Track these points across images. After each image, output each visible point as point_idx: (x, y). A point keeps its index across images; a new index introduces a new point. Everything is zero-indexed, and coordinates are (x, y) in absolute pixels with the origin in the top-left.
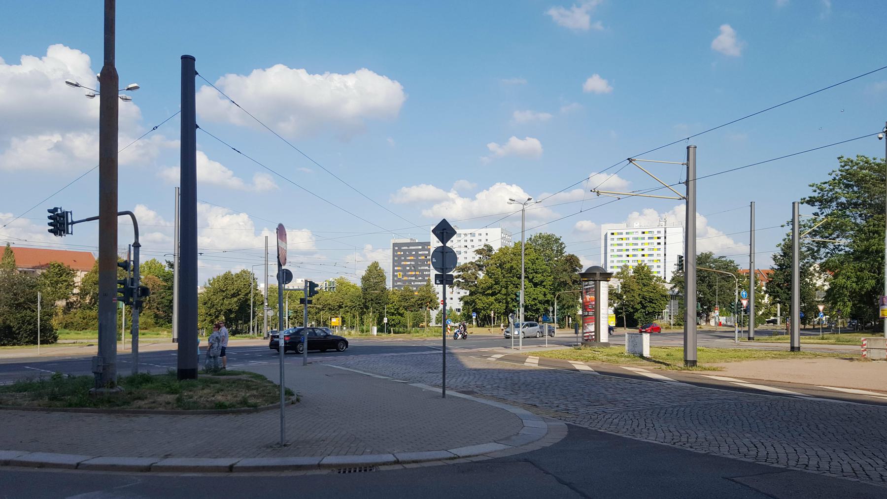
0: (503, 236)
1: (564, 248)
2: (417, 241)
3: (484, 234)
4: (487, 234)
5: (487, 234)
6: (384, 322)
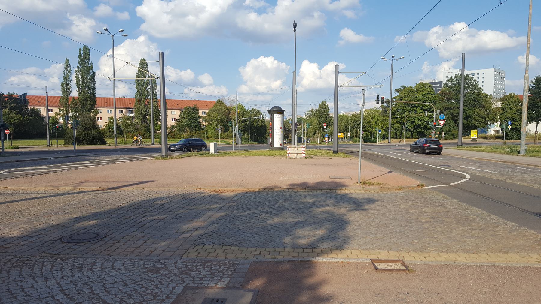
0: (496, 74)
1: (477, 83)
2: (437, 81)
3: (481, 74)
4: (483, 73)
5: (483, 73)
6: (349, 136)
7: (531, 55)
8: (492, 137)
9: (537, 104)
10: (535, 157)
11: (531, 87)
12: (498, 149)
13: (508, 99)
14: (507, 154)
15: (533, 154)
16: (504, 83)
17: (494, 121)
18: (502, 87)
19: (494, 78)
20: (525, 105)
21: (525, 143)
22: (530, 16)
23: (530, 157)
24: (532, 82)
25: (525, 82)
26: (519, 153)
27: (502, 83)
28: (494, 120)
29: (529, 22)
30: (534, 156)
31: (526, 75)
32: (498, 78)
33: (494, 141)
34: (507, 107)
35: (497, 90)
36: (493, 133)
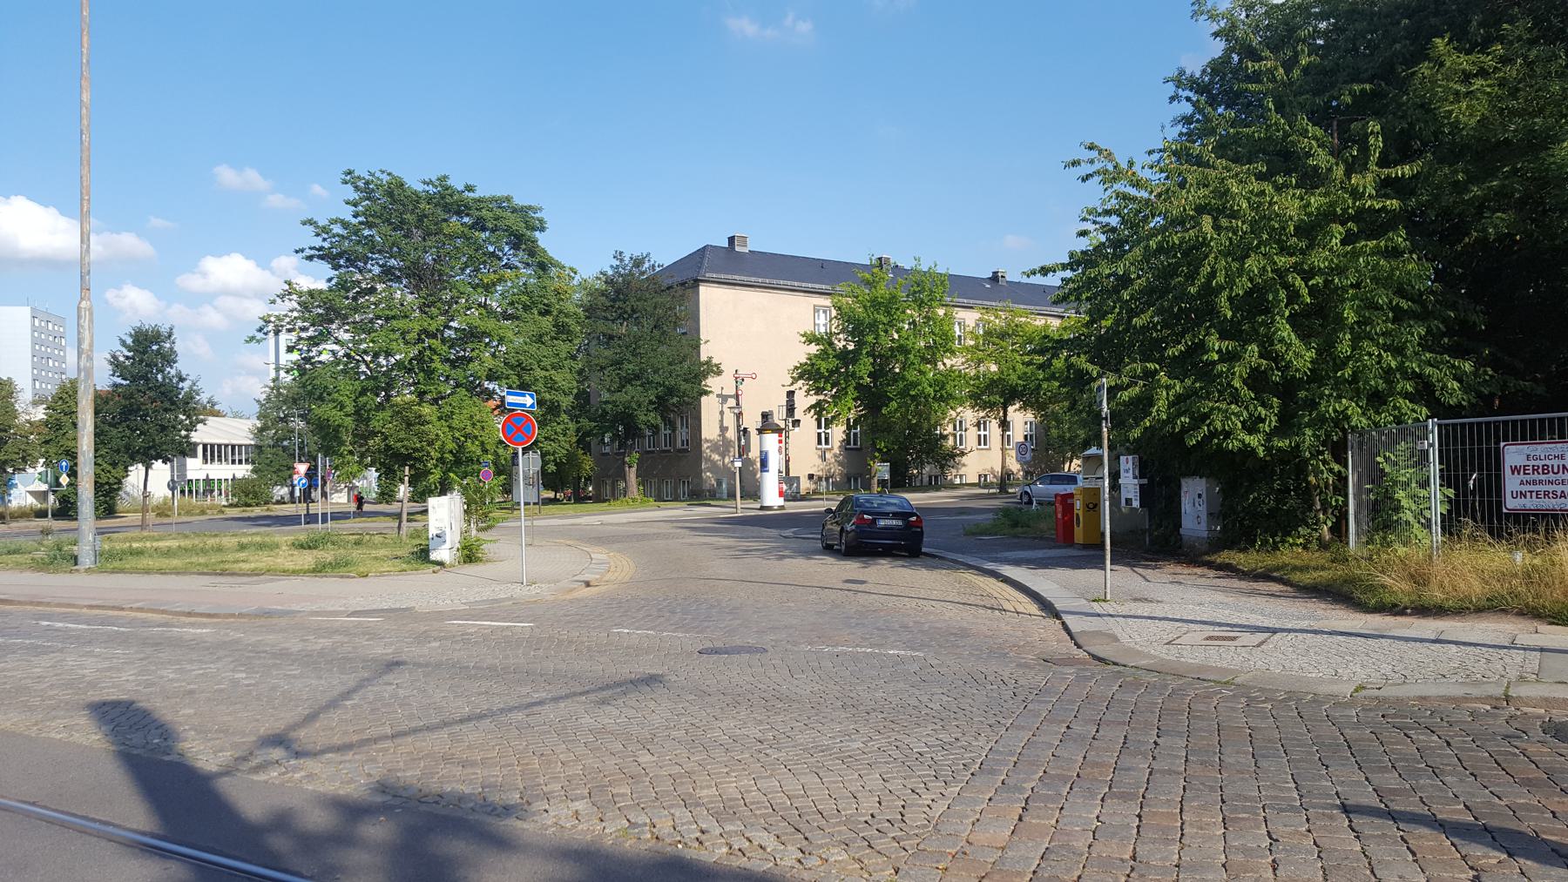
7: (98, 233)
8: (23, 514)
9: (143, 408)
10: (125, 573)
11: (122, 359)
12: (15, 552)
13: (65, 396)
14: (40, 570)
15: (124, 562)
16: (62, 353)
17: (24, 459)
18: (56, 364)
19: (33, 336)
20: (84, 402)
21: (94, 531)
22: (84, 111)
23: (113, 572)
24: (123, 343)
25: (82, 327)
26: (76, 564)
27: (56, 352)
28: (26, 460)
29: (82, 131)
30: (122, 571)
31: (84, 304)
32: (49, 350)
33: (27, 527)
34: (64, 419)
35: (43, 373)
36: (31, 500)
